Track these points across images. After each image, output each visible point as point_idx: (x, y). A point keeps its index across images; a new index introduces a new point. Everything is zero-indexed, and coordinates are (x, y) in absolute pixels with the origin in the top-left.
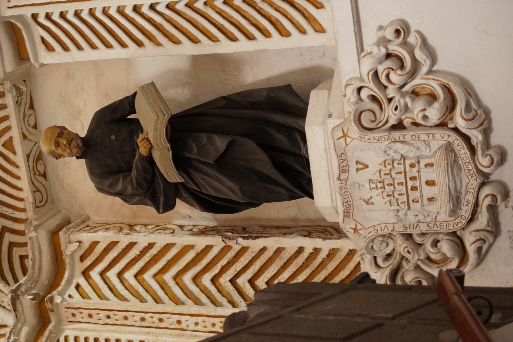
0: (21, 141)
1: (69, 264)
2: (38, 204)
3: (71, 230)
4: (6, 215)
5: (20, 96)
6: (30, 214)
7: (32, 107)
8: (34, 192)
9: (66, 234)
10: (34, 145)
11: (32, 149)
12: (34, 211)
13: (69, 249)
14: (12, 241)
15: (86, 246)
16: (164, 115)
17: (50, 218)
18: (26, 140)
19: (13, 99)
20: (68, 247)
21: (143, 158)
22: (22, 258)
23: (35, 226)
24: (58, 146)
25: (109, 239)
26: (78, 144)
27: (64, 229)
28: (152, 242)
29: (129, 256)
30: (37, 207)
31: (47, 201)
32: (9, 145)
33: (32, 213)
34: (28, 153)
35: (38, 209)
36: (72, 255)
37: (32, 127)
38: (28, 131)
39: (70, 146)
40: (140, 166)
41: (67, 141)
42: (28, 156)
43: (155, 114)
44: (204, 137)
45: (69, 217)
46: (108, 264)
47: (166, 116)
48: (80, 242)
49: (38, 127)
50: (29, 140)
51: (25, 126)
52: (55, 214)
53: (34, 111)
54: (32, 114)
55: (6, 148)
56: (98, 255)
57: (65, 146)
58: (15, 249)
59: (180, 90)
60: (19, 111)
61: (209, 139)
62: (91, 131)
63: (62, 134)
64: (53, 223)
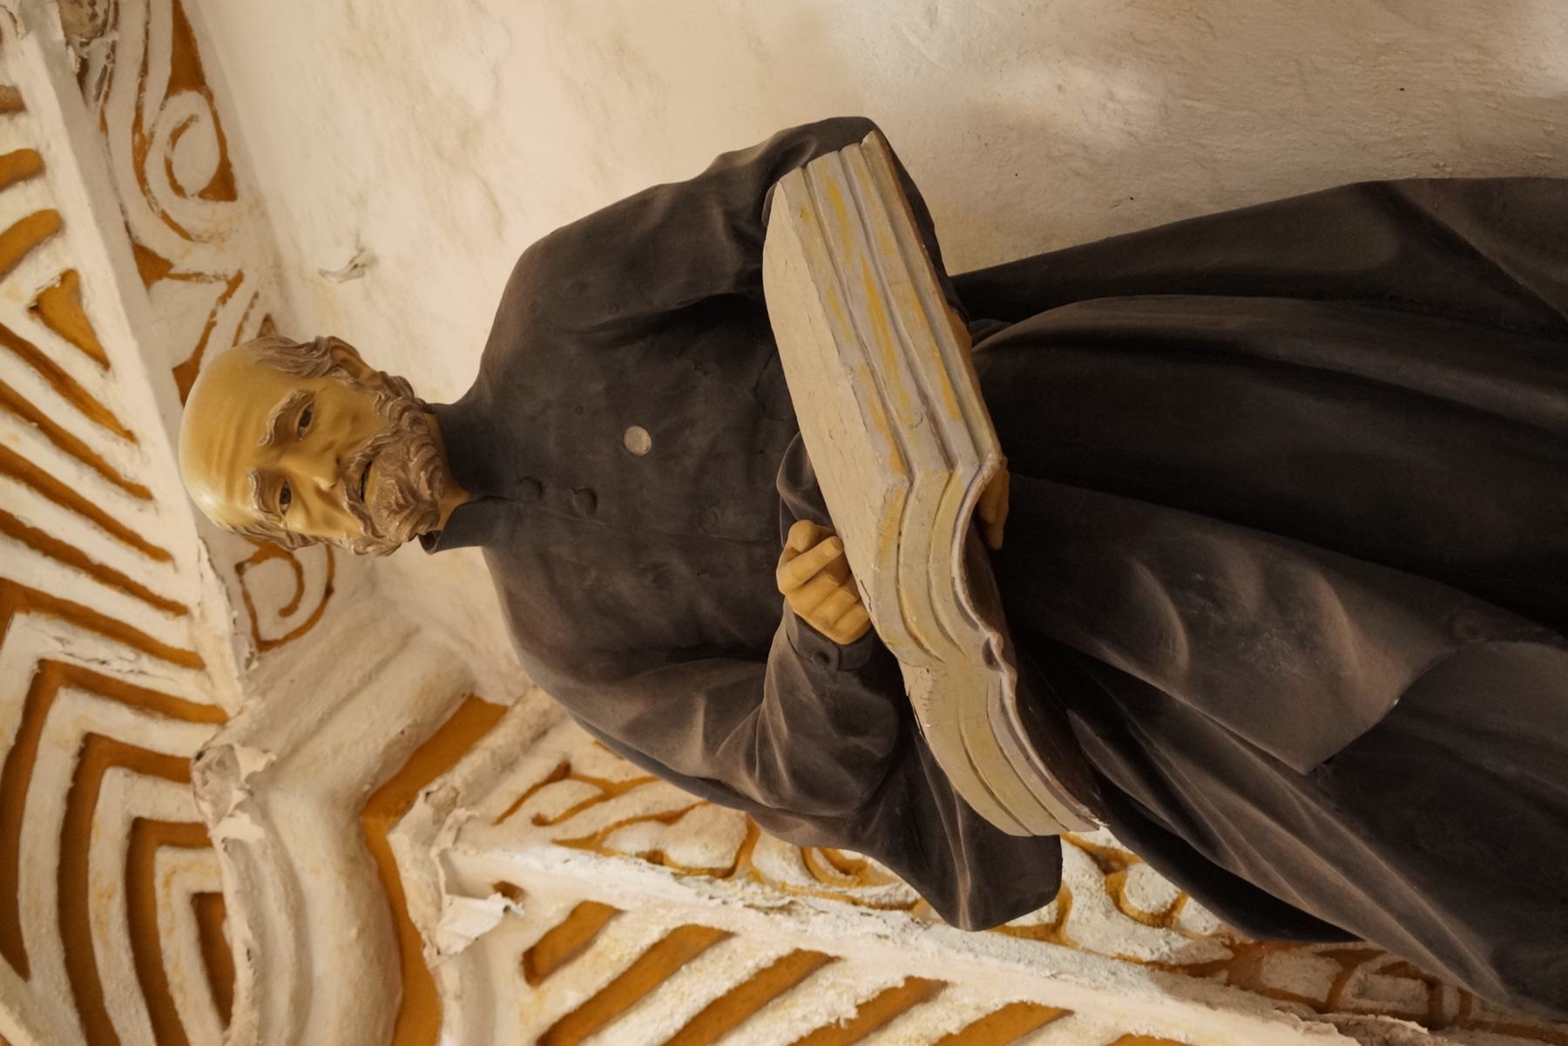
0: (126, 301)
1: (458, 997)
2: (270, 631)
3: (460, 813)
4: (96, 675)
5: (101, 31)
6: (223, 683)
7: (189, 72)
8: (239, 568)
9: (429, 841)
10: (223, 299)
11: (211, 325)
12: (247, 678)
13: (453, 928)
14: (145, 813)
15: (547, 913)
16: (950, 463)
17: (351, 695)
18: (163, 286)
19: (52, 60)
20: (448, 912)
21: (825, 658)
22: (206, 907)
23: (249, 779)
24: (286, 497)
25: (675, 913)
26: (409, 491)
27: (421, 809)
28: (927, 974)
29: (798, 1013)
30: (263, 645)
31: (329, 591)
32: (59, 305)
33: (239, 687)
34: (186, 354)
35: (274, 658)
36: (477, 950)
37: (203, 195)
38: (175, 227)
39: (359, 496)
40: (808, 693)
41: (340, 473)
42: (185, 375)
43: (888, 449)
44: (1241, 567)
45: (464, 671)
46: (679, 1022)
47: (963, 471)
48: (508, 890)
49: (241, 186)
50: (185, 277)
51: (152, 203)
52: (383, 665)
53: (210, 97)
54: (192, 118)
55: (49, 323)
56: (622, 967)
57: (327, 498)
58: (165, 859)
59: (1084, 79)
60: (104, 126)
61: (1279, 595)
62: (504, 368)
63: (305, 421)
64: (365, 733)
